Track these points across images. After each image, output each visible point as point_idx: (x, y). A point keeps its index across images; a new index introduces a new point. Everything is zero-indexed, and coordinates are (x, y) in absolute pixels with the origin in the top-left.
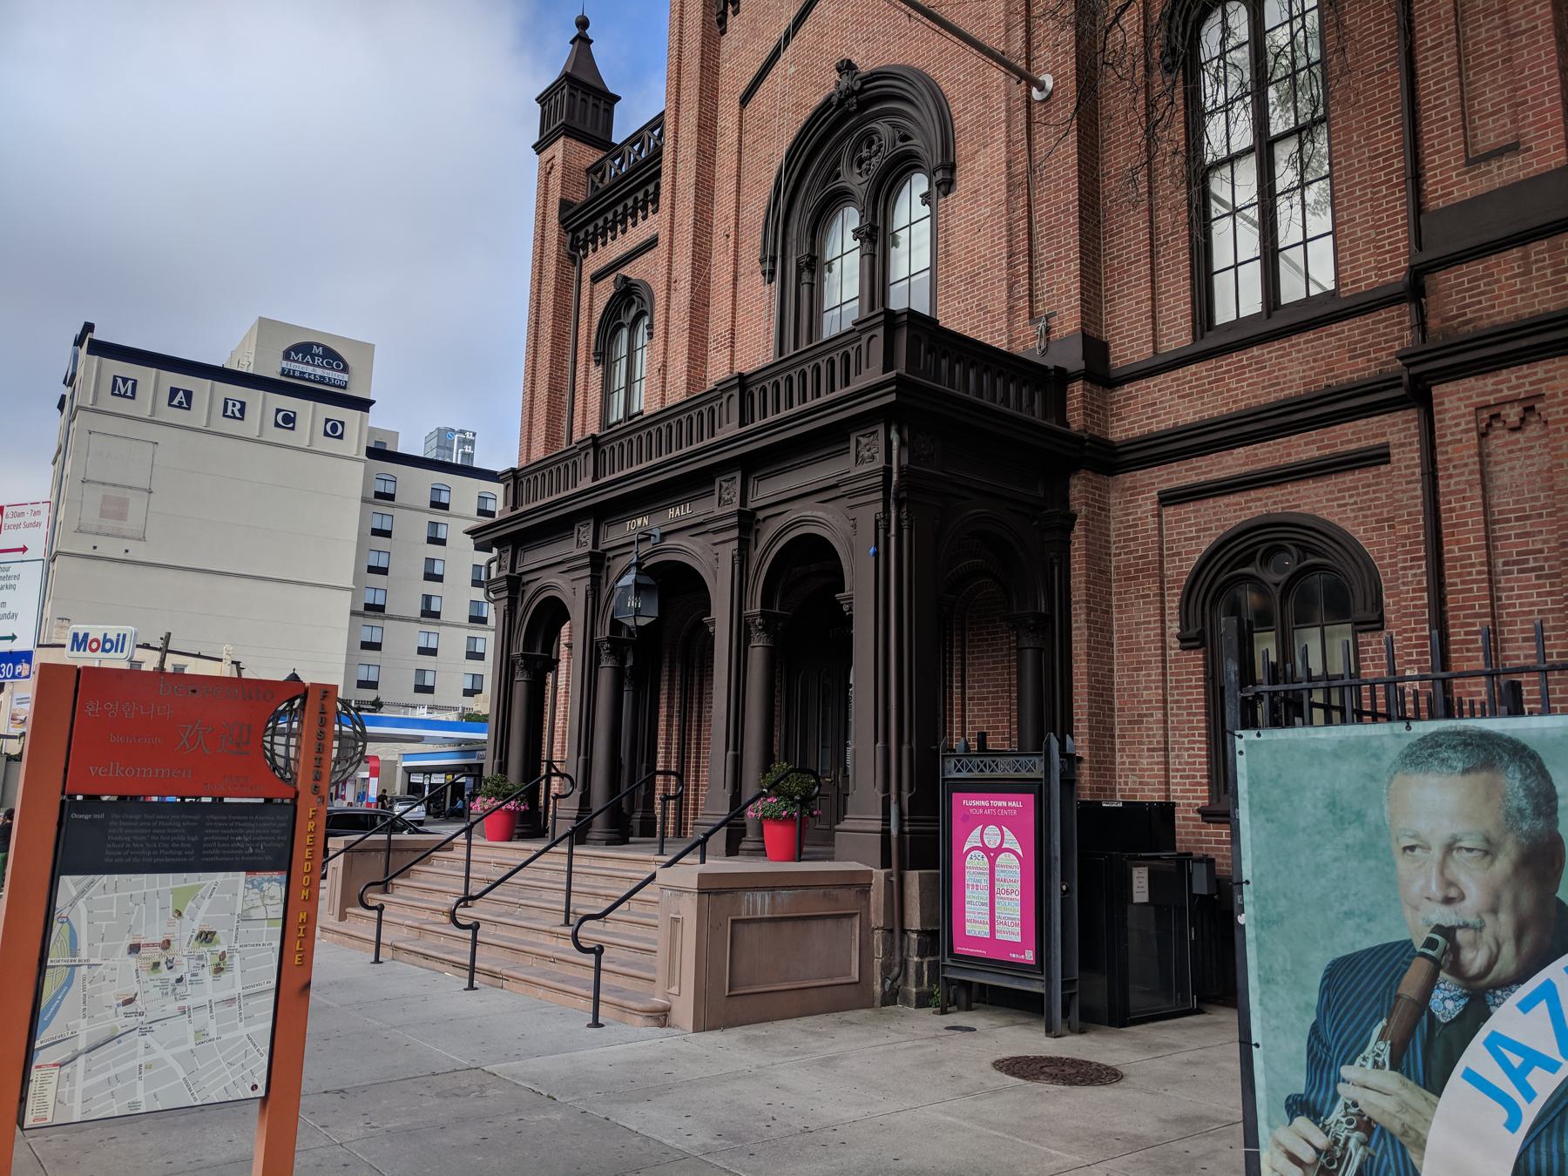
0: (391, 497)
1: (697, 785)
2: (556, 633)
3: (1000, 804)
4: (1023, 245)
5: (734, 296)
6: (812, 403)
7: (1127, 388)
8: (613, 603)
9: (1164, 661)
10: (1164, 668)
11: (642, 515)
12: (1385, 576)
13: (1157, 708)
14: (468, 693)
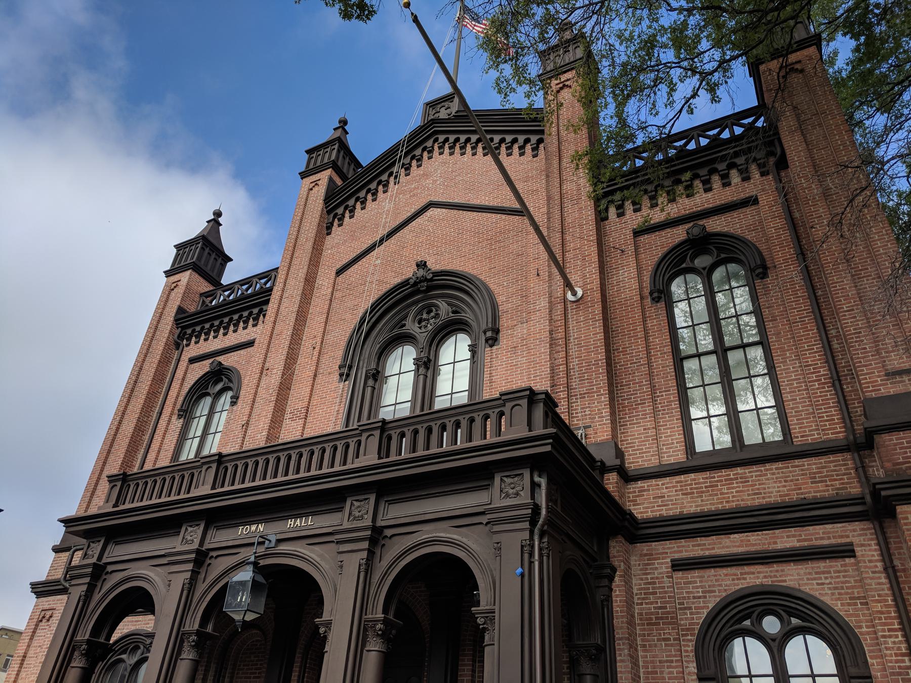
7: (640, 484)
11: (258, 522)
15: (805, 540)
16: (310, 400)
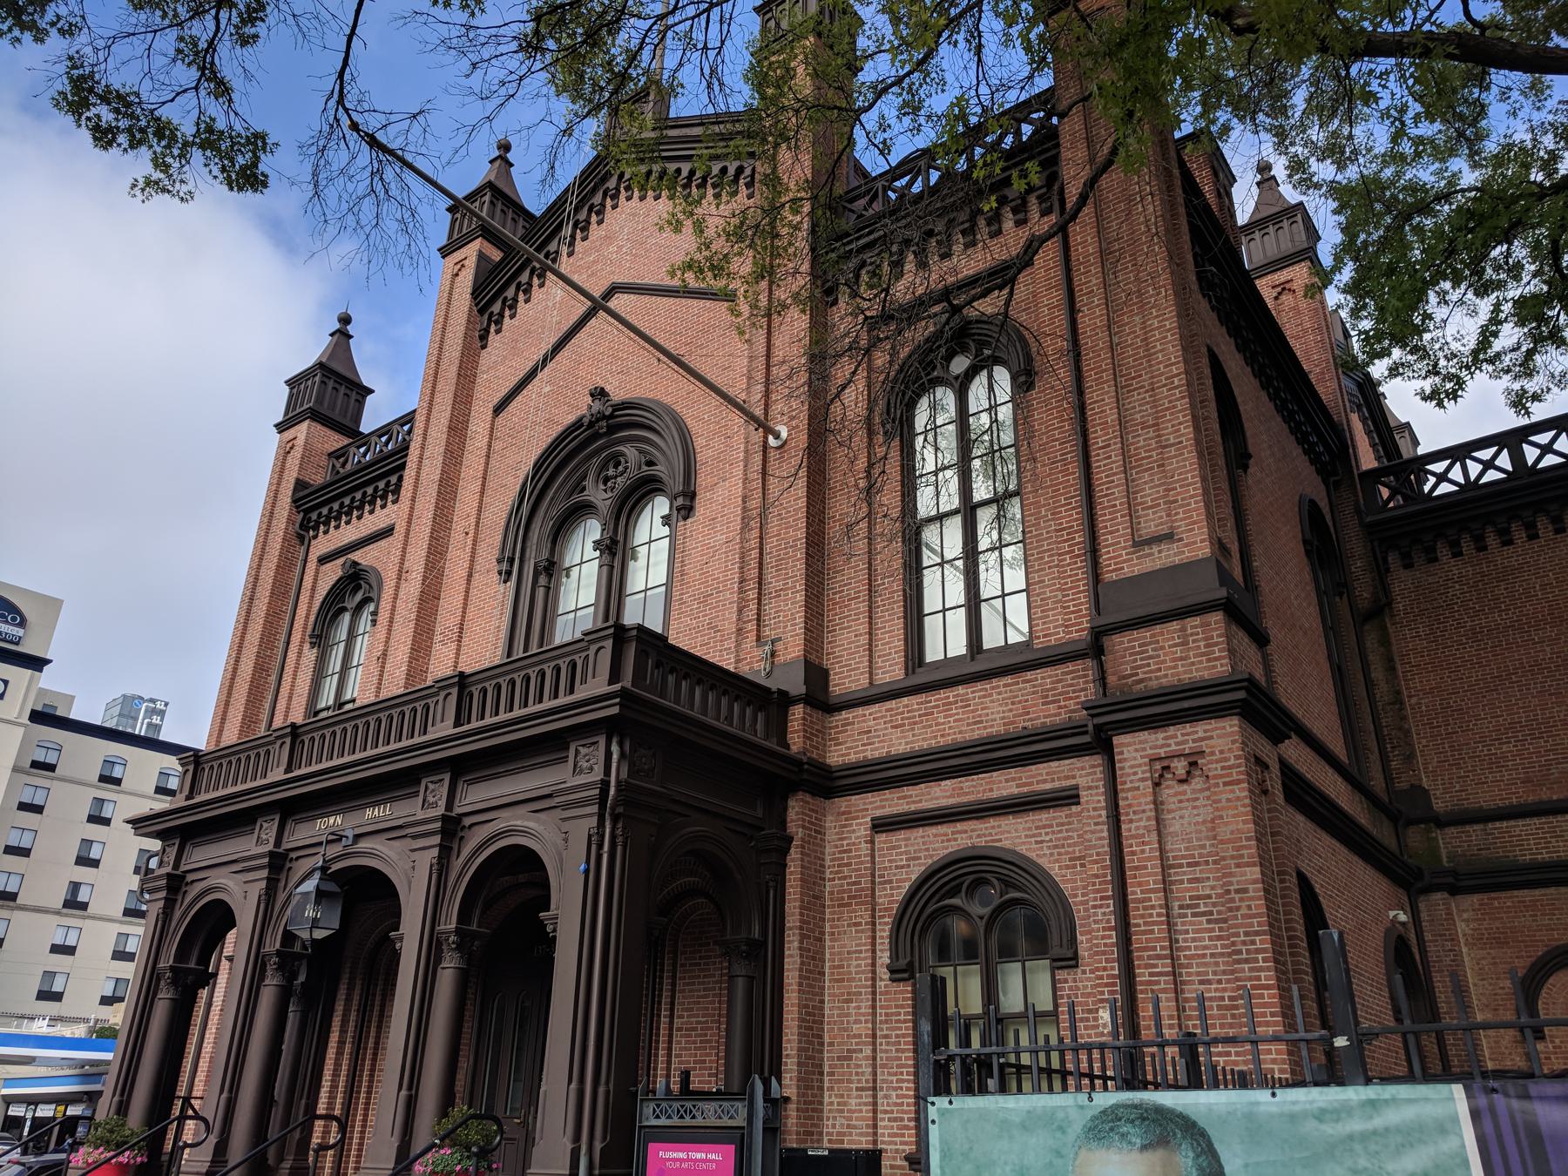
0: (51, 768)
1: (364, 1126)
2: (221, 937)
3: (699, 1156)
4: (754, 573)
5: (467, 592)
6: (533, 708)
8: (289, 912)
9: (874, 993)
10: (874, 1000)
11: (335, 813)
12: (1079, 913)
13: (865, 1043)
14: (106, 1001)
15: (1026, 784)
16: (464, 612)
